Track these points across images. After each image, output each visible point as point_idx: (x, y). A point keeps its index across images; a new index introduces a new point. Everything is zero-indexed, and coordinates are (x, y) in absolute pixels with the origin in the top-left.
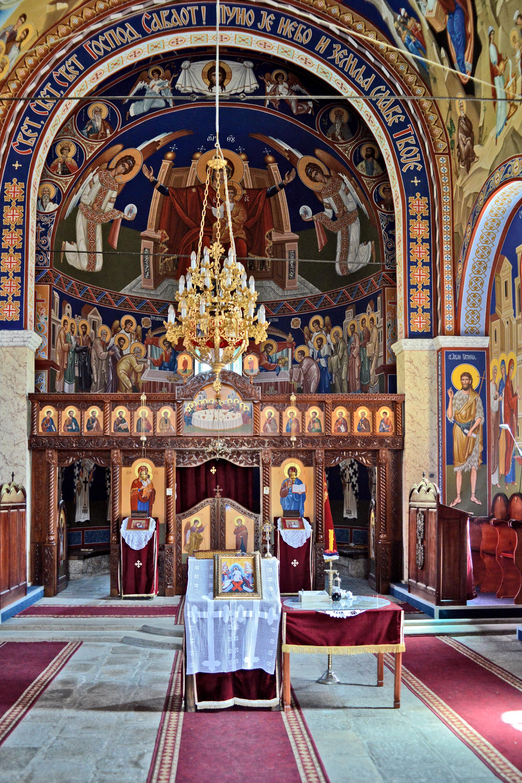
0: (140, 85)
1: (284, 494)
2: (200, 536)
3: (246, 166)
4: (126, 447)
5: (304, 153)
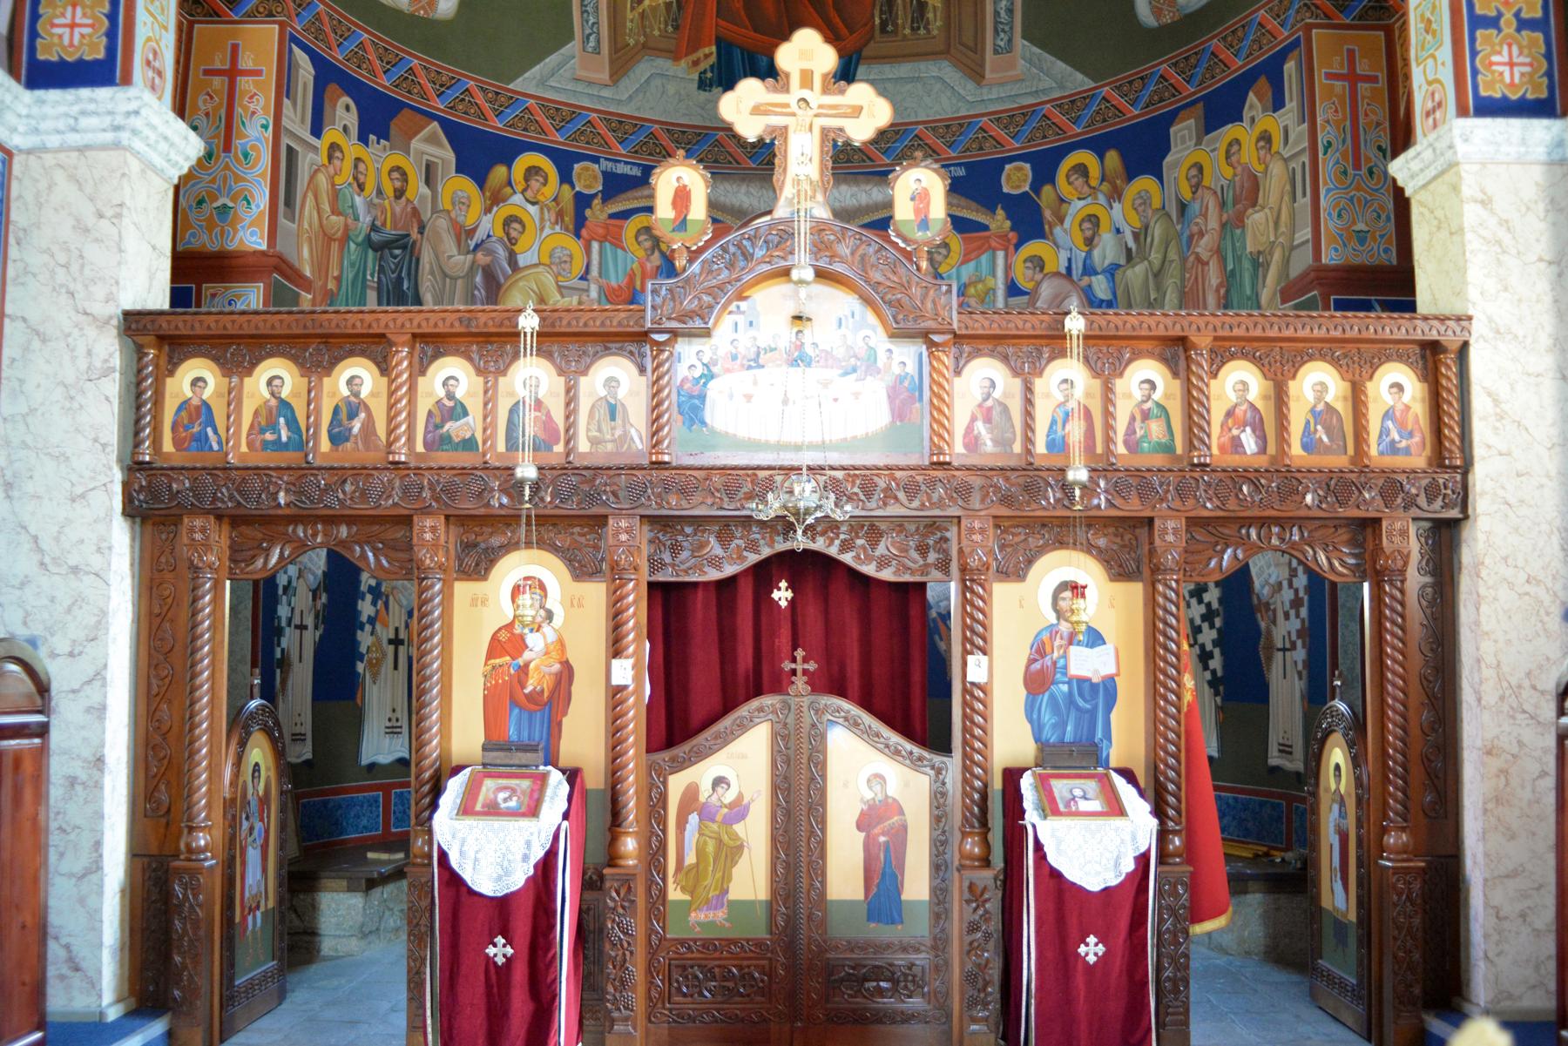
1: (1037, 682)
2: (736, 837)
4: (468, 506)
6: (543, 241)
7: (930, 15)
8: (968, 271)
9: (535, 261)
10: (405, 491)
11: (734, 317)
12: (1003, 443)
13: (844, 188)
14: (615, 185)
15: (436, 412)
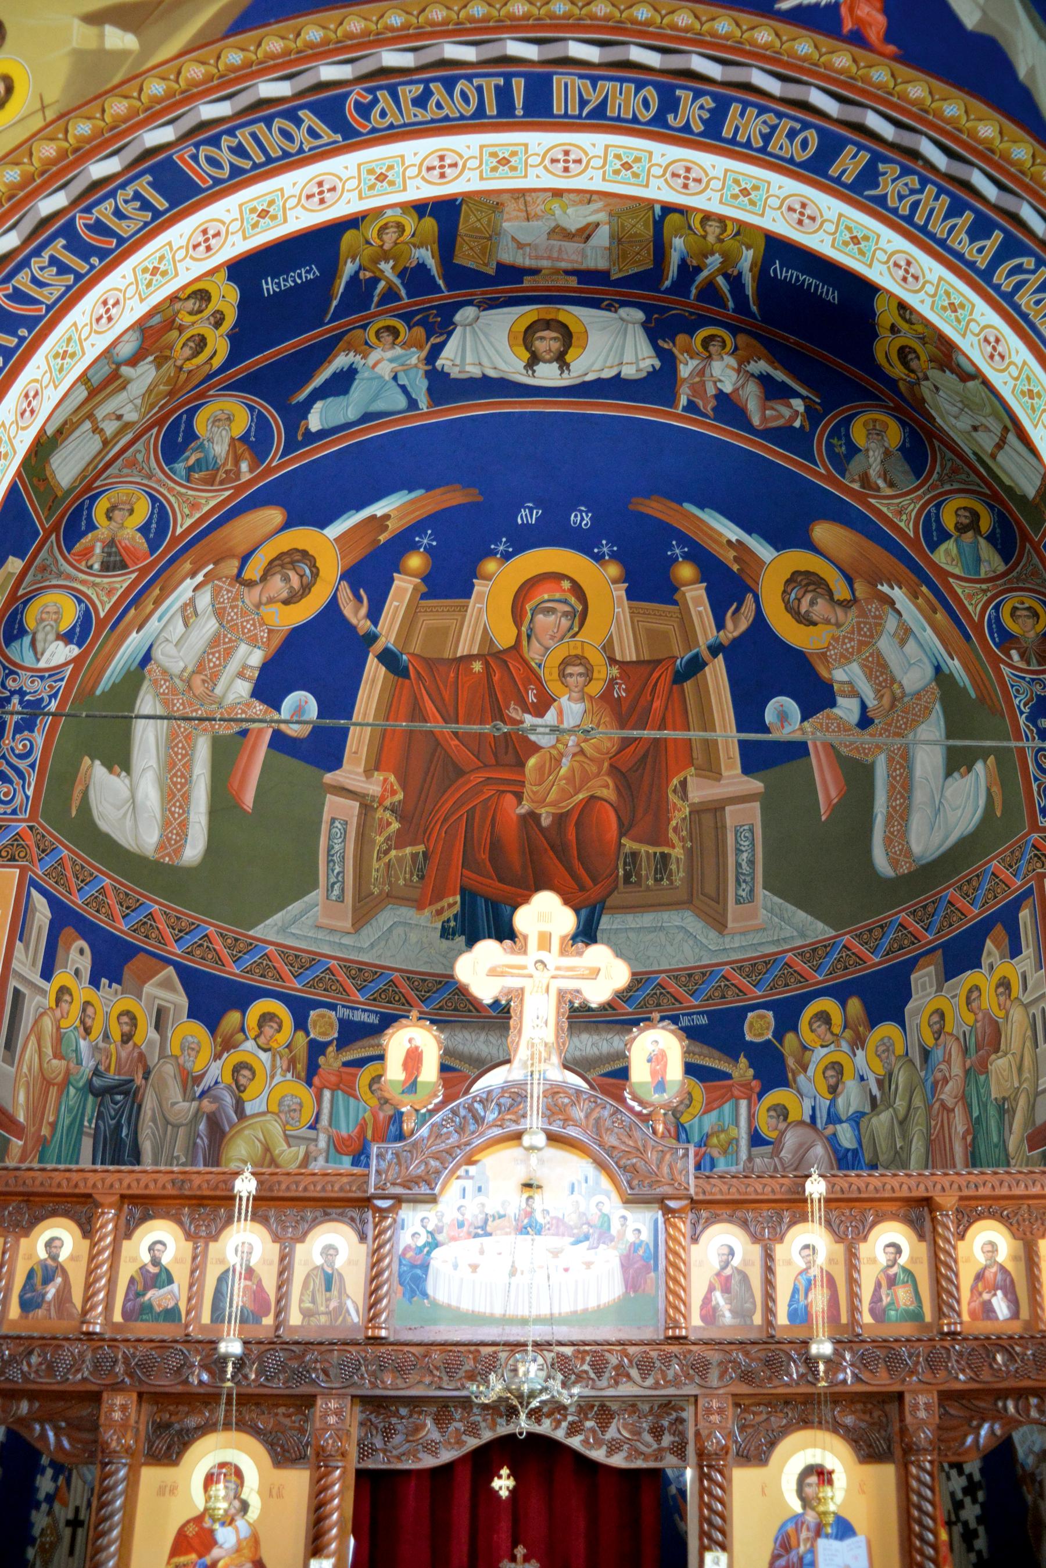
0: (340, 361)
3: (619, 598)
4: (165, 1383)
5: (779, 541)
6: (273, 1089)
7: (674, 867)
8: (710, 1121)
9: (263, 1108)
10: (97, 1366)
11: (460, 1182)
12: (742, 1314)
13: (585, 1036)
14: (351, 1033)
15: (139, 1278)
